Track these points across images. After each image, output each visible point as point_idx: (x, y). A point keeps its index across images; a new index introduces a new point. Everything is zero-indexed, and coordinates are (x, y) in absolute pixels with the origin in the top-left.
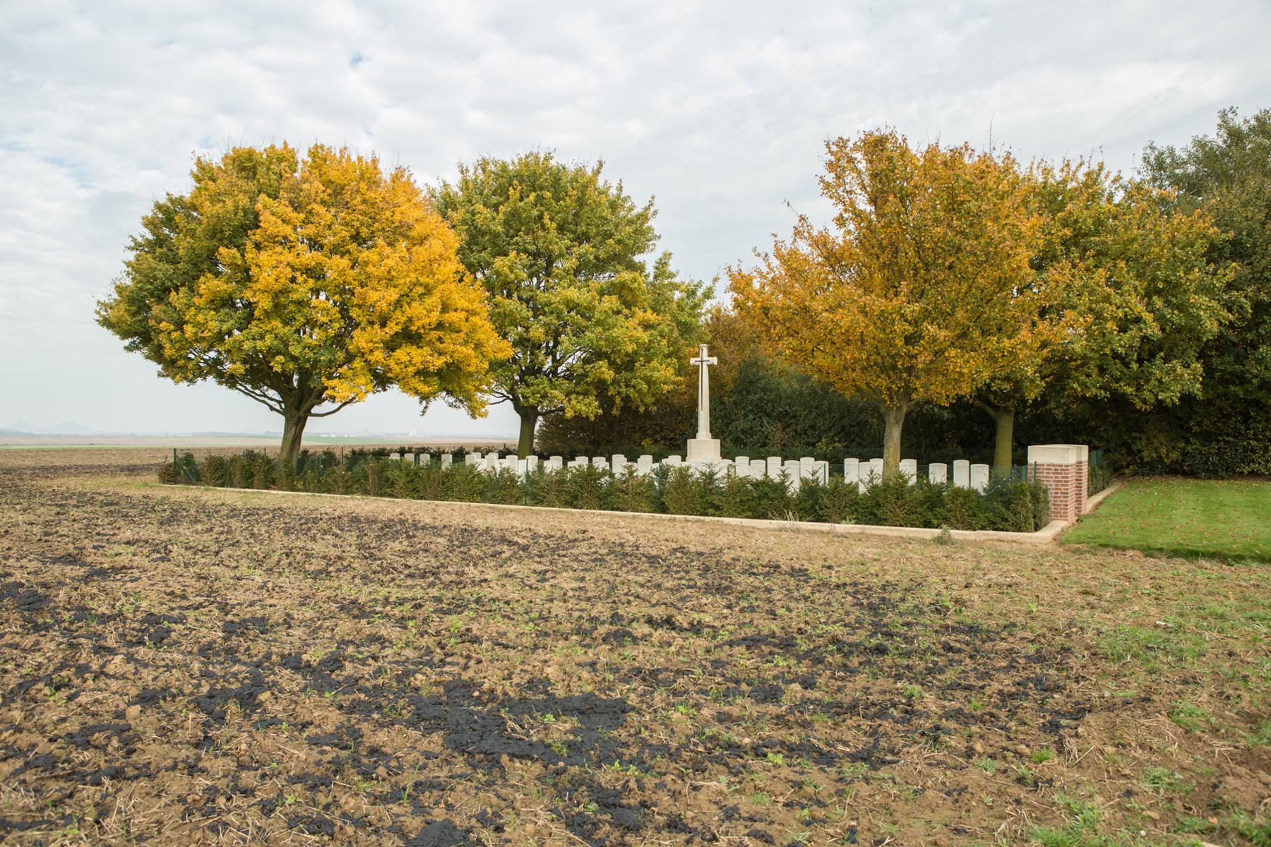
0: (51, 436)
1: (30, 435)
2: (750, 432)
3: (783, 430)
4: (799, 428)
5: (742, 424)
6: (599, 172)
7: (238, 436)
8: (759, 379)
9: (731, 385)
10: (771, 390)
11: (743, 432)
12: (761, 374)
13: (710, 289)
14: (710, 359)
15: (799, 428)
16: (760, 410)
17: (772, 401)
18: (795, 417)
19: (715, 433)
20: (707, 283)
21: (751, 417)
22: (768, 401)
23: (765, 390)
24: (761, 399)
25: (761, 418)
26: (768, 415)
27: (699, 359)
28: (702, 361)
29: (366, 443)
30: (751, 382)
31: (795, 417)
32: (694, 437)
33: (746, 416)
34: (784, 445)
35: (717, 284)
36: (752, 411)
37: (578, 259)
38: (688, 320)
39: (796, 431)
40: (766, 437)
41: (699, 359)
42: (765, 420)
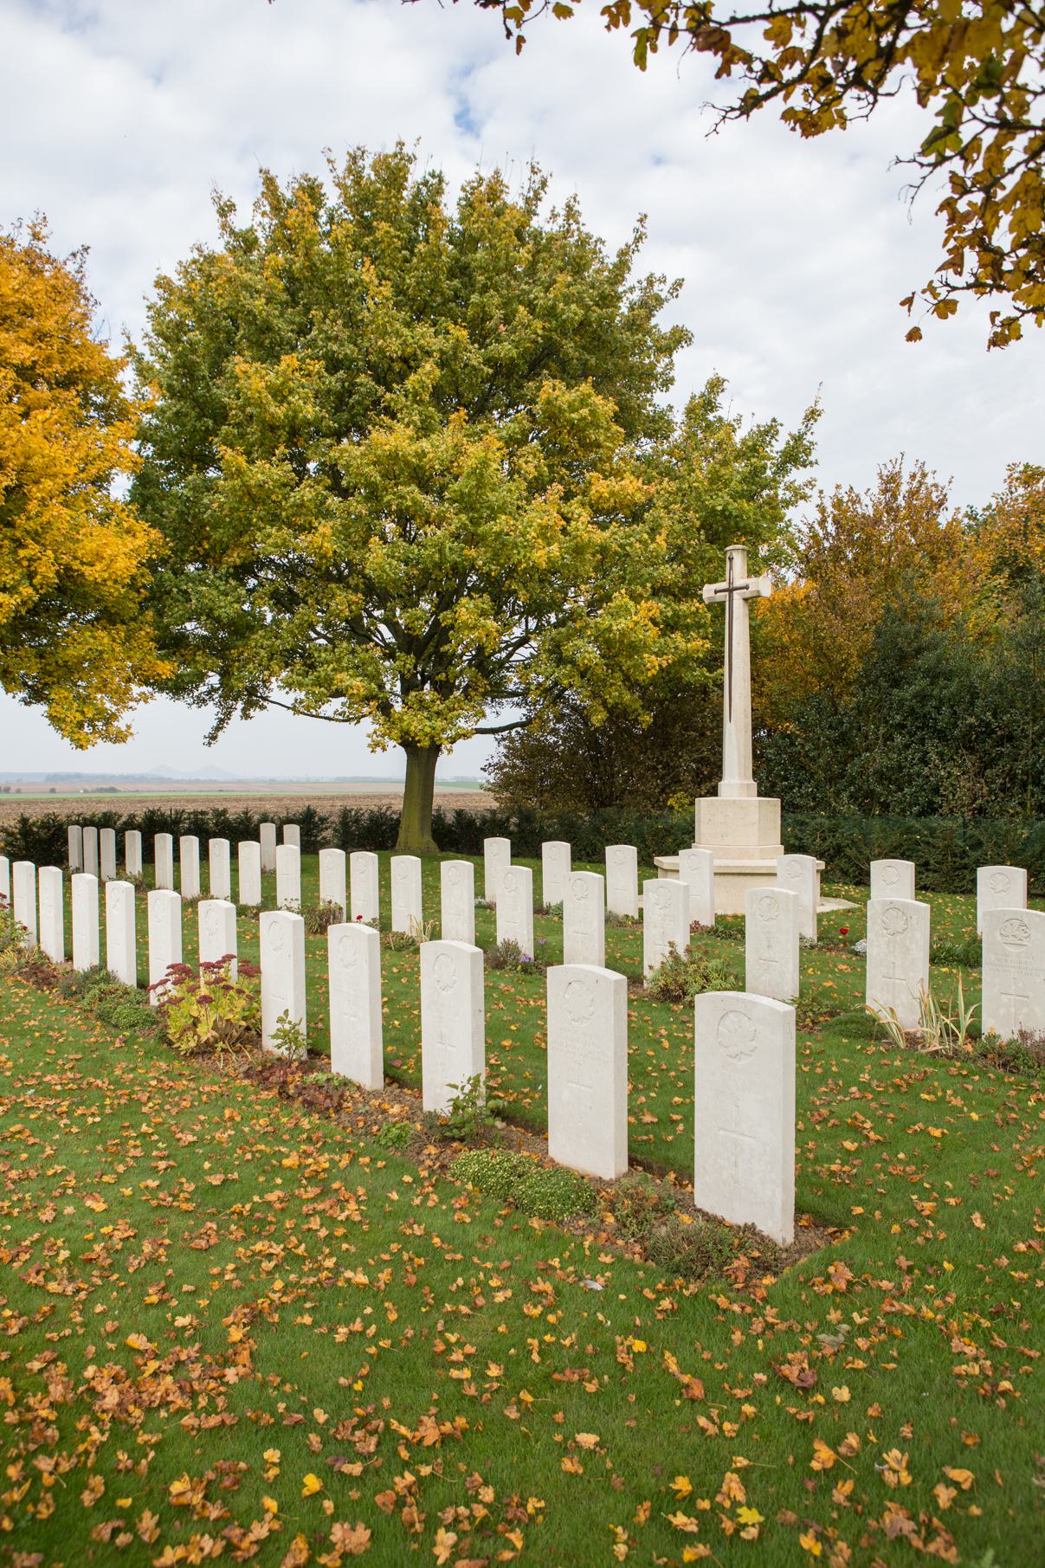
0: (190, 782)
1: (169, 781)
2: (893, 777)
3: (980, 774)
4: (1019, 768)
5: (879, 759)
6: (537, 198)
7: (385, 781)
8: (919, 651)
9: (857, 666)
10: (949, 676)
11: (881, 776)
12: (926, 638)
13: (798, 439)
14: (752, 581)
15: (1019, 768)
16: (919, 722)
17: (953, 702)
18: (1010, 738)
19: (768, 780)
20: (791, 425)
21: (899, 739)
22: (941, 702)
23: (934, 675)
24: (922, 697)
25: (922, 741)
26: (942, 735)
27: (724, 585)
28: (730, 591)
29: (124, 791)
30: (902, 658)
31: (1010, 738)
32: (714, 792)
33: (889, 738)
34: (981, 810)
35: (816, 427)
36: (901, 726)
37: (442, 364)
38: (733, 506)
39: (1011, 776)
40: (936, 791)
41: (724, 585)
42: (932, 748)
